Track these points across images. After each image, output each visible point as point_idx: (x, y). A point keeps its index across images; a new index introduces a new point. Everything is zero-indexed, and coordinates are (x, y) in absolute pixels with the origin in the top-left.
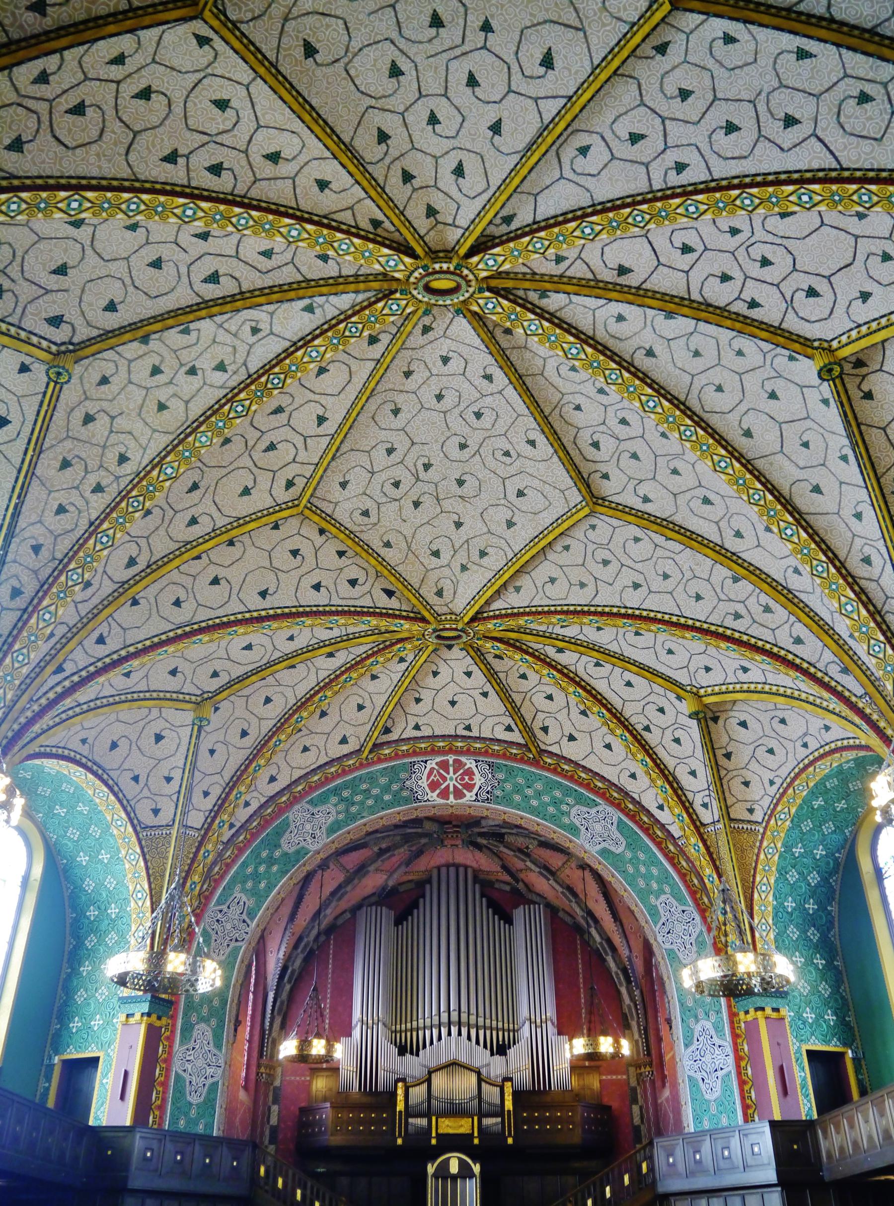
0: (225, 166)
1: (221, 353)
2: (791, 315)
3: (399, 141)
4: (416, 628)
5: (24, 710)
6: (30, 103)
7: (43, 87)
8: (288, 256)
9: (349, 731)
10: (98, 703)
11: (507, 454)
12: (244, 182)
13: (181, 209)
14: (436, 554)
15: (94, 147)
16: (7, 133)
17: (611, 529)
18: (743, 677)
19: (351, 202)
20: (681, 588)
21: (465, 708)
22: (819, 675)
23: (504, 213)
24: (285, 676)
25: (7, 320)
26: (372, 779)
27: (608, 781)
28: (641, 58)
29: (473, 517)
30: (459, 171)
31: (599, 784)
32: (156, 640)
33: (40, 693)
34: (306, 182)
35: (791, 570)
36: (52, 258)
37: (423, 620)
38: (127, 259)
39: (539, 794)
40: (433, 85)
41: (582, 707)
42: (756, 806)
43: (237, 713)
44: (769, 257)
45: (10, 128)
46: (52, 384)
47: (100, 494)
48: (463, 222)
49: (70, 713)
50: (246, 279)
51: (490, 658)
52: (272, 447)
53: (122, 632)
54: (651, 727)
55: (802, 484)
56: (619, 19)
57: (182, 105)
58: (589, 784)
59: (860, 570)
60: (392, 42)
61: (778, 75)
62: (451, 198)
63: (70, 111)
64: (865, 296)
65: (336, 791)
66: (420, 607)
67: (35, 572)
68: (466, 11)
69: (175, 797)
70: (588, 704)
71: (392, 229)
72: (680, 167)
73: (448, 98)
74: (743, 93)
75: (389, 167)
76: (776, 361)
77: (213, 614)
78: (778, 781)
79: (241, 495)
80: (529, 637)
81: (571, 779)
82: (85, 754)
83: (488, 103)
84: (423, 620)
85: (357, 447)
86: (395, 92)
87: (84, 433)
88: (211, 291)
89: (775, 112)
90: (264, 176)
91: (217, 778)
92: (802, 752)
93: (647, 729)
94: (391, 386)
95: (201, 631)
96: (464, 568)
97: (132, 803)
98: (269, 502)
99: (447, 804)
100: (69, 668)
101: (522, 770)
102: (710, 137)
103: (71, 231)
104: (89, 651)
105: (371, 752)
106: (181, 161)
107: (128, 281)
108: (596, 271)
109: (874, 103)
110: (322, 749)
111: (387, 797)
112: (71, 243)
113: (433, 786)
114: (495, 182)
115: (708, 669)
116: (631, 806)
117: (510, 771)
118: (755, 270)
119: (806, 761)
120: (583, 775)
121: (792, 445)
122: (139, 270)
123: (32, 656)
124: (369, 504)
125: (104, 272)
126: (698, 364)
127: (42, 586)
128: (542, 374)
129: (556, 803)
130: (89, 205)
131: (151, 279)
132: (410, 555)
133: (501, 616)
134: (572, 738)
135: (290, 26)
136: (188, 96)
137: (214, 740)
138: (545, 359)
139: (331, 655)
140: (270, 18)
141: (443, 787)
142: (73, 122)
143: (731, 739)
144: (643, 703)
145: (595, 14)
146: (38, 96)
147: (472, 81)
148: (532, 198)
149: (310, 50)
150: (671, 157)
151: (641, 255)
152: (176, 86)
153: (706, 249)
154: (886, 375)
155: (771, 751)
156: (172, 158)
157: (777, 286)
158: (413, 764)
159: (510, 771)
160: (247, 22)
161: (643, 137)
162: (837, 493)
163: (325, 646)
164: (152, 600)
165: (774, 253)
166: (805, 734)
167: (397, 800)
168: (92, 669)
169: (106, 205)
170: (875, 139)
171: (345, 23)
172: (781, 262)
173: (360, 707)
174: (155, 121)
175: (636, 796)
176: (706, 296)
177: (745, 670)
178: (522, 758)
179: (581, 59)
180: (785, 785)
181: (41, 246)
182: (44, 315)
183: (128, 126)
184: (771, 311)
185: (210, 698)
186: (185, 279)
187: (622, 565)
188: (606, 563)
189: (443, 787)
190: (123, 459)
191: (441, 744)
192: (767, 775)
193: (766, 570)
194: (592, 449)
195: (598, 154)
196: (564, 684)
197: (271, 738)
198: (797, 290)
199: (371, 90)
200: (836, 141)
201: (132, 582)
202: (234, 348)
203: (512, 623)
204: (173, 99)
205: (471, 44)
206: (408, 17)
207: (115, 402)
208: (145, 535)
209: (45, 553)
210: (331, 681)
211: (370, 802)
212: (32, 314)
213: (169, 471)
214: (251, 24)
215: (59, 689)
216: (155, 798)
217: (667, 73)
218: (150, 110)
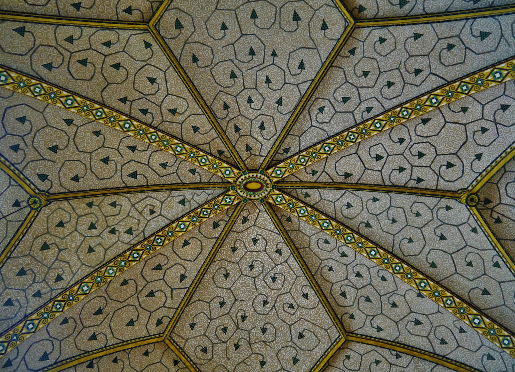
0: (149, 111)
1: (131, 223)
2: (441, 181)
3: (233, 111)
6: (61, 50)
7: (70, 44)
8: (175, 168)
11: (291, 306)
12: (157, 121)
13: (123, 122)
15: (87, 83)
16: (46, 59)
19: (209, 140)
23: (284, 146)
25: (16, 165)
28: (343, 57)
29: (272, 357)
30: (262, 127)
34: (188, 126)
35: (485, 358)
36: (51, 140)
38: (90, 153)
40: (250, 84)
44: (422, 151)
45: (48, 57)
47: (38, 298)
48: (264, 153)
50: (151, 178)
52: (151, 294)
55: (475, 291)
56: (332, 39)
57: (133, 76)
60: (232, 61)
61: (407, 52)
62: (258, 141)
68: (265, 47)
71: (229, 156)
72: (369, 110)
73: (257, 90)
74: (393, 66)
75: (228, 123)
76: (439, 213)
79: (128, 325)
83: (275, 90)
85: (203, 298)
86: (233, 85)
87: (39, 255)
88: (131, 182)
89: (409, 70)
90: (167, 120)
94: (224, 257)
98: (144, 333)
102: (381, 92)
103: (64, 126)
106: (128, 103)
107: (88, 166)
108: (333, 178)
109: (455, 47)
114: (279, 129)
118: (416, 161)
121: (462, 267)
122: (95, 162)
124: (207, 343)
126: (396, 227)
128: (309, 247)
130: (77, 105)
131: (101, 168)
135: (188, 46)
136: (136, 73)
138: (310, 237)
140: (179, 40)
142: (80, 67)
145: (321, 40)
146: (66, 48)
147: (268, 81)
149: (195, 59)
150: (364, 106)
151: (355, 165)
152: (132, 67)
153: (389, 155)
154: (505, 206)
156: (124, 100)
157: (430, 167)
160: (169, 39)
161: (349, 99)
162: (499, 291)
165: (424, 148)
169: (85, 108)
170: (461, 63)
171: (212, 50)
172: (430, 153)
174: (119, 81)
176: (393, 181)
179: (317, 62)
181: (47, 130)
183: (105, 79)
184: (430, 181)
186: (119, 173)
190: (59, 278)
193: (468, 364)
194: (342, 298)
195: (329, 111)
198: (441, 166)
199: (222, 83)
200: (442, 72)
202: (139, 220)
204: (130, 72)
205: (267, 63)
206: (240, 50)
207: (64, 240)
208: (60, 338)
212: (30, 168)
213: (85, 288)
214: (170, 40)
217: (356, 64)
218: (118, 75)
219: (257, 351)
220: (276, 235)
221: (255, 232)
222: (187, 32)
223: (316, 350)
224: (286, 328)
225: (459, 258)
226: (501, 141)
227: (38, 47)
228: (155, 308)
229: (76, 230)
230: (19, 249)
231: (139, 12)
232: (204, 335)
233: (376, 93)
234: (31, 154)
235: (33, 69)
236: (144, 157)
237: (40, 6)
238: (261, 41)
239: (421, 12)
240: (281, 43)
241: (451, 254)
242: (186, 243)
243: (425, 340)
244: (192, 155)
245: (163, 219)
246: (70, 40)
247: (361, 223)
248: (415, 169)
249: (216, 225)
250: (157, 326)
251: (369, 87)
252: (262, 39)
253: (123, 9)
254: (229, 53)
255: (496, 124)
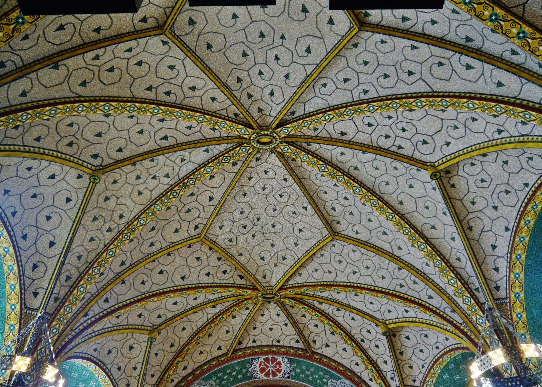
0: (172, 92)
1: (168, 170)
2: (416, 152)
3: (246, 82)
4: (254, 293)
5: (68, 335)
6: (91, 67)
7: (97, 61)
8: (198, 128)
9: (222, 344)
10: (103, 331)
11: (294, 213)
14: (263, 259)
15: (117, 85)
17: (342, 246)
18: (406, 315)
20: (375, 273)
21: (277, 332)
22: (441, 313)
24: (193, 317)
26: (233, 367)
27: (345, 367)
30: (272, 94)
31: (341, 369)
32: (132, 300)
33: (76, 327)
35: (424, 264)
37: (257, 289)
39: (312, 374)
40: (260, 59)
41: (332, 331)
42: (416, 379)
43: (169, 335)
44: (405, 128)
46: (92, 183)
48: (274, 114)
49: (90, 336)
51: (288, 307)
52: (189, 211)
53: (116, 296)
54: (365, 340)
55: (427, 225)
58: (336, 368)
59: (456, 264)
60: (244, 43)
63: (107, 70)
64: (448, 144)
65: (215, 374)
66: (255, 283)
67: (78, 268)
69: (137, 378)
70: (335, 329)
72: (365, 92)
77: (159, 287)
78: (426, 366)
79: (175, 232)
80: (306, 297)
81: (327, 366)
82: (96, 356)
84: (257, 289)
85: (227, 210)
87: (104, 205)
88: (164, 143)
90: (189, 96)
91: (158, 368)
92: (436, 351)
93: (362, 340)
94: (242, 184)
95: (154, 296)
96: (275, 265)
97: (117, 381)
98: (187, 236)
99: (269, 380)
100: (91, 314)
101: (304, 362)
104: (101, 306)
105: (232, 354)
106: (153, 90)
107: (128, 139)
108: (331, 134)
110: (209, 353)
111: (240, 376)
112: (104, 123)
113: (262, 370)
115: (389, 311)
116: (357, 379)
117: (298, 363)
118: (399, 133)
119: (439, 356)
120: (333, 364)
121: (421, 208)
123: (74, 308)
124: (232, 236)
125: (118, 136)
126: (378, 173)
127: (81, 275)
128: (309, 178)
129: (321, 378)
131: (138, 138)
132: (251, 259)
133: (292, 287)
134: (327, 346)
135: (201, 37)
136: (157, 64)
137: (158, 349)
139: (214, 307)
140: (193, 34)
141: (267, 371)
143: (402, 345)
144: (360, 328)
147: (277, 58)
148: (303, 105)
149: (209, 46)
150: (361, 88)
151: (350, 127)
152: (153, 61)
153: (378, 125)
154: (460, 177)
155: (421, 351)
156: (149, 89)
158: (252, 359)
159: (298, 363)
161: (349, 80)
163: (211, 302)
164: (131, 281)
166: (437, 342)
167: (245, 378)
168: (101, 314)
172: (411, 131)
173: (227, 332)
175: (359, 374)
177: (407, 311)
178: (304, 356)
180: (429, 368)
181: (91, 125)
182: (90, 154)
183: (131, 76)
184: (408, 150)
185: (157, 328)
186: (153, 139)
187: (348, 263)
188: (340, 262)
189: (267, 371)
190: (121, 216)
191: (266, 349)
192: (421, 363)
195: (331, 86)
196: (323, 319)
197: (185, 347)
199: (235, 62)
201: (122, 273)
202: (173, 167)
203: (298, 291)
204: (151, 65)
206: (250, 34)
209: (83, 259)
210: (214, 319)
211: (232, 379)
213: (142, 222)
215: (85, 324)
216: (128, 378)
219: (269, 238)
220: (283, 170)
221: (266, 167)
222: (199, 26)
223: (310, 241)
224: (290, 226)
225: (420, 202)
226: (466, 140)
227: (72, 72)
228: (192, 219)
229: (126, 182)
230: (89, 206)
231: (153, 19)
232: (230, 231)
233: (373, 80)
234: (82, 144)
235: (72, 92)
236: (172, 125)
237: (66, 42)
238: (270, 26)
239: (420, 31)
240: (289, 29)
241: (415, 198)
242: (212, 177)
243: (389, 245)
244: (212, 122)
245: (192, 164)
246: (97, 57)
247: (473, 284)
248: (398, 139)
249: (234, 164)
250: (195, 230)
251: (367, 74)
252: (272, 25)
253: (139, 20)
254: (241, 36)
255: (465, 127)
